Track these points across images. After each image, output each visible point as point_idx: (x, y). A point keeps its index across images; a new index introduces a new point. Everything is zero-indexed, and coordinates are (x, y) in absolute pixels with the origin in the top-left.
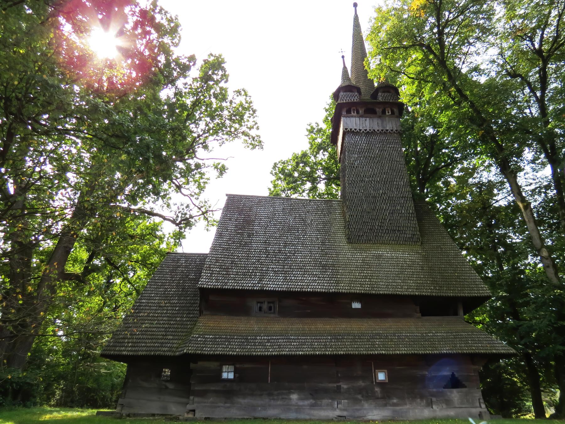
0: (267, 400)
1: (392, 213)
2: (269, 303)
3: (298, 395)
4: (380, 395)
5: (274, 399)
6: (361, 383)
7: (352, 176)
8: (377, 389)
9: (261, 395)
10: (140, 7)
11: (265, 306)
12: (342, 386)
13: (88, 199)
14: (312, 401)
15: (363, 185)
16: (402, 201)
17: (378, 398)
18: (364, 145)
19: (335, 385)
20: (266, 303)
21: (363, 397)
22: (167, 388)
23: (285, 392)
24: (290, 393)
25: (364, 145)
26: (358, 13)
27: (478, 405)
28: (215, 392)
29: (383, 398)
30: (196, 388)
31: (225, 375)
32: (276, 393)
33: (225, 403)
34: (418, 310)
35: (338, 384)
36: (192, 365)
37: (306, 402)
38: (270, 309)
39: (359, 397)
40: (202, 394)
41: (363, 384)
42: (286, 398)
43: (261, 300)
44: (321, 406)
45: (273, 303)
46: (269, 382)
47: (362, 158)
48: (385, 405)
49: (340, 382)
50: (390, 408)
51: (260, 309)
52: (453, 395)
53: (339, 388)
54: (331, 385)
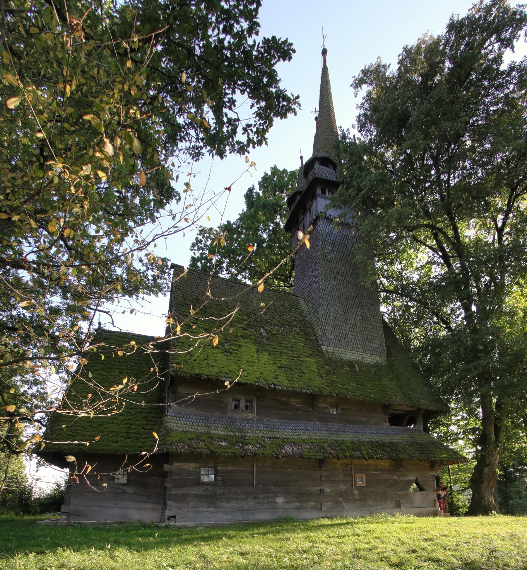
0: (253, 504)
1: (362, 320)
2: (246, 401)
3: (284, 498)
4: (358, 498)
5: (259, 503)
6: (343, 487)
7: (325, 270)
8: (356, 492)
9: (247, 499)
10: (170, 488)
11: (242, 405)
12: (326, 489)
13: (189, 303)
14: (297, 504)
15: (335, 284)
16: (372, 308)
17: (356, 500)
18: (338, 237)
19: (319, 489)
20: (243, 401)
21: (343, 499)
22: (125, 492)
23: (271, 495)
24: (276, 496)
25: (338, 237)
26: (327, 65)
27: (319, 508)
28: (197, 496)
29: (361, 500)
30: (173, 493)
31: (205, 479)
32: (261, 496)
33: (208, 507)
34: (387, 419)
35: (322, 488)
36: (166, 467)
37: (292, 506)
38: (247, 407)
39: (341, 499)
40: (183, 498)
41: (344, 488)
42: (272, 502)
43: (238, 397)
44: (306, 508)
45: (250, 402)
46: (255, 485)
47: (335, 252)
48: (362, 506)
49: (323, 486)
50: (366, 509)
51: (236, 407)
52: (416, 497)
53: (322, 491)
54: (315, 488)
